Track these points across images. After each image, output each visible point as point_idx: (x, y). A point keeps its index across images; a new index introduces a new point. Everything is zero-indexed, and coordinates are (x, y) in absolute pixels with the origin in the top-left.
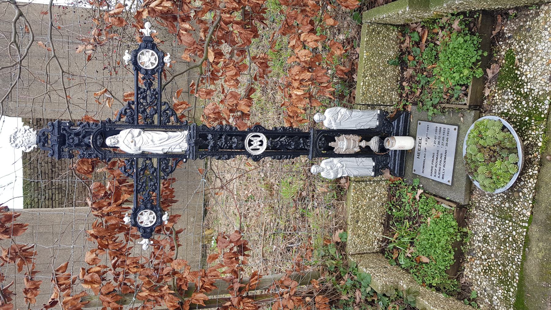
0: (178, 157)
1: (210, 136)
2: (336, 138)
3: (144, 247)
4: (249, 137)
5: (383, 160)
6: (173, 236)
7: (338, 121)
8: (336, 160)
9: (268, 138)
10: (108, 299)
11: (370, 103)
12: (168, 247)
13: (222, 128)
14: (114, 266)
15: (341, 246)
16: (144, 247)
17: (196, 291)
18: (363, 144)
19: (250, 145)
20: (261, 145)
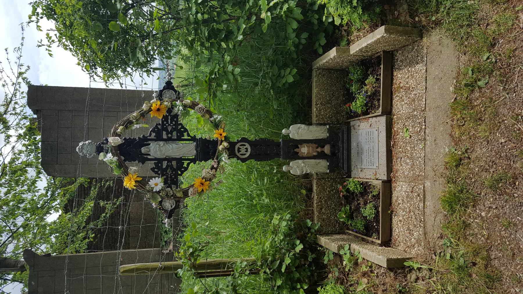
2: (299, 146)
8: (300, 161)
11: (322, 122)
18: (319, 150)
19: (239, 151)
20: (247, 151)
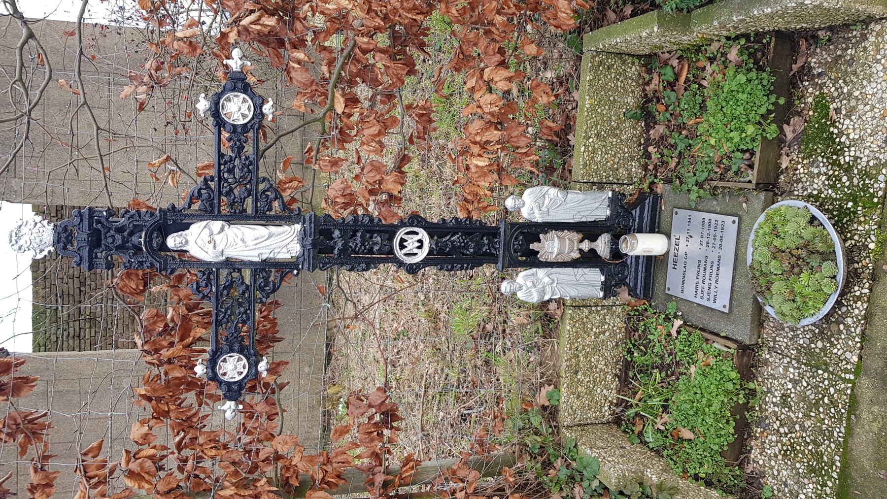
0: (284, 268)
1: (337, 233)
3: (228, 415)
4: (401, 234)
5: (616, 270)
7: (544, 209)
8: (541, 272)
9: (431, 236)
14: (179, 447)
15: (550, 413)
16: (228, 415)
18: (586, 246)
19: (402, 247)
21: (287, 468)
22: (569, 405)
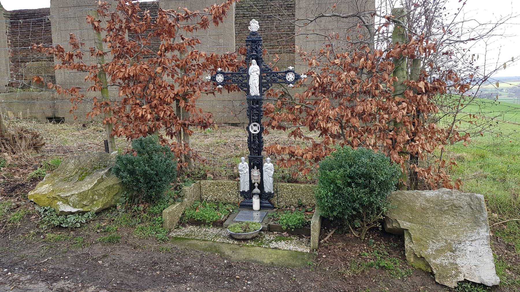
0: (248, 92)
1: (258, 106)
3: (207, 77)
4: (258, 125)
5: (248, 195)
6: (212, 91)
7: (267, 170)
8: (248, 170)
9: (258, 134)
10: (184, 63)
12: (206, 89)
13: (262, 111)
14: (198, 65)
15: (205, 177)
16: (207, 77)
17: (185, 102)
18: (256, 185)
19: (254, 125)
21: (191, 95)
22: (206, 183)
